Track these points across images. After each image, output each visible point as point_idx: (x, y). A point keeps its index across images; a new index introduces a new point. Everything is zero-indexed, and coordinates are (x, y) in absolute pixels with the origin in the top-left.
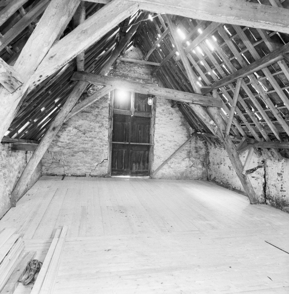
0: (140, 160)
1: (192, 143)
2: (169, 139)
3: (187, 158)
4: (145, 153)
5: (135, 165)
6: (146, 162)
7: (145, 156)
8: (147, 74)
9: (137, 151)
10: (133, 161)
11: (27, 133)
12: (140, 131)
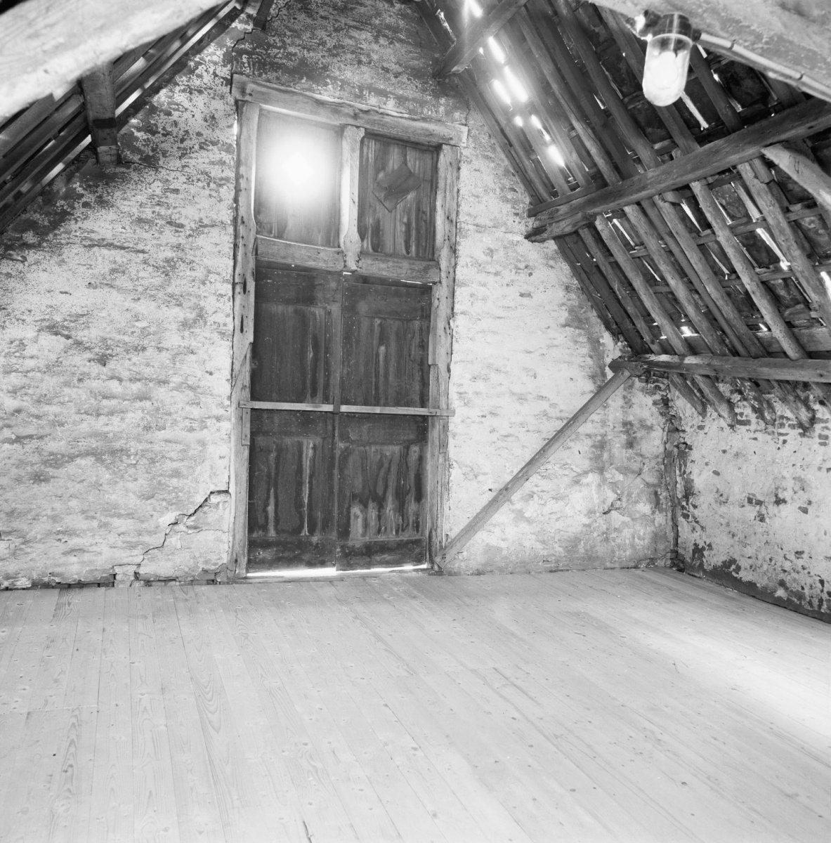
0: (386, 487)
4: (405, 455)
6: (411, 498)
12: (383, 348)
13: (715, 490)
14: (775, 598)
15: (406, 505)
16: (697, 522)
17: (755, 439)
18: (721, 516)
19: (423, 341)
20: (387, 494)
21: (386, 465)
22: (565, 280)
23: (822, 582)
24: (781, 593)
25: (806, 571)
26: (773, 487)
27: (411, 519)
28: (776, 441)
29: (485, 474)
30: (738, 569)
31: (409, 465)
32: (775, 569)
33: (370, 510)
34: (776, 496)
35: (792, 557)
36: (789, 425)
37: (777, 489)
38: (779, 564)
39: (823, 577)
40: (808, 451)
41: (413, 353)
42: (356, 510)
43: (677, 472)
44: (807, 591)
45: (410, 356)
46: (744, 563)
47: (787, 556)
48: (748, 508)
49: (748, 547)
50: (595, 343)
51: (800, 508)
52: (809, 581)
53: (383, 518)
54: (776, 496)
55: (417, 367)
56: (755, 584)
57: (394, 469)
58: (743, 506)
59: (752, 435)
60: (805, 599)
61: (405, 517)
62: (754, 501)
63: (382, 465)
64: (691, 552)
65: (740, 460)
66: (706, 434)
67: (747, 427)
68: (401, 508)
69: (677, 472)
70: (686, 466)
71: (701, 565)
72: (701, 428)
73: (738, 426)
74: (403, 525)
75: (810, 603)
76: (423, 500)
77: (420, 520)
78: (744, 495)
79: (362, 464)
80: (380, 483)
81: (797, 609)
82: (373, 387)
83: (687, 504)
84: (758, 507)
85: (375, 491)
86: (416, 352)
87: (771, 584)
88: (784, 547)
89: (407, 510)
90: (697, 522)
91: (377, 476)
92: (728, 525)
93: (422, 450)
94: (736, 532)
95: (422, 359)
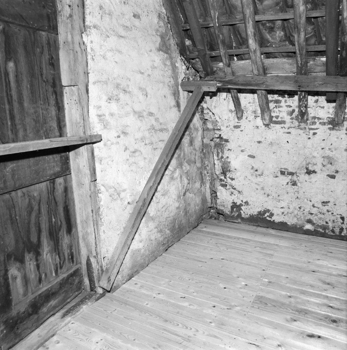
0: (39, 231)
1: (271, 137)
2: (138, 108)
3: (63, 86)
4: (52, 190)
5: (19, 270)
6: (63, 232)
7: (56, 203)
8: (18, 313)
9: (15, 190)
10: (9, 256)
11: (310, 6)
12: (11, 65)
13: (251, 167)
14: (304, 230)
15: (60, 241)
16: (235, 189)
17: (289, 133)
18: (256, 184)
19: (52, 58)
20: (42, 239)
21: (36, 208)
22: (157, 8)
23: (343, 218)
24: (308, 227)
25: (330, 213)
26: (304, 163)
27: (66, 252)
28: (308, 133)
29: (124, 190)
30: (272, 215)
31: (57, 199)
32: (304, 214)
33: (27, 263)
34: (307, 169)
35: (320, 205)
36: (320, 123)
37: (308, 164)
38: (307, 210)
39: (343, 215)
40: (336, 139)
41: (44, 72)
42: (14, 271)
43: (216, 158)
44: (330, 225)
45: (42, 75)
46: (275, 211)
47: (315, 205)
48: (282, 177)
49: (281, 201)
50: (174, 68)
51: (328, 175)
52: (333, 218)
53: (41, 265)
54: (307, 169)
55: (51, 90)
56: (286, 223)
57: (44, 210)
58: (277, 177)
59: (286, 130)
60: (328, 229)
61: (61, 255)
62: (286, 173)
63: (32, 209)
64: (230, 207)
65: (274, 148)
66: (242, 131)
67: (282, 125)
68: (56, 248)
69: (216, 158)
70: (223, 153)
71: (239, 216)
72: (236, 127)
73: (272, 125)
74: (60, 263)
75: (333, 231)
76: (74, 230)
77: (73, 250)
78: (278, 169)
79: (11, 216)
80: (33, 229)
81: (324, 235)
82: (8, 118)
83: (225, 178)
84: (290, 177)
85: (29, 239)
86: (47, 71)
87: (300, 222)
88: (312, 200)
89: (62, 246)
90: (235, 189)
91: (29, 223)
92: (263, 189)
93: (65, 181)
94: (270, 193)
95: (54, 80)
